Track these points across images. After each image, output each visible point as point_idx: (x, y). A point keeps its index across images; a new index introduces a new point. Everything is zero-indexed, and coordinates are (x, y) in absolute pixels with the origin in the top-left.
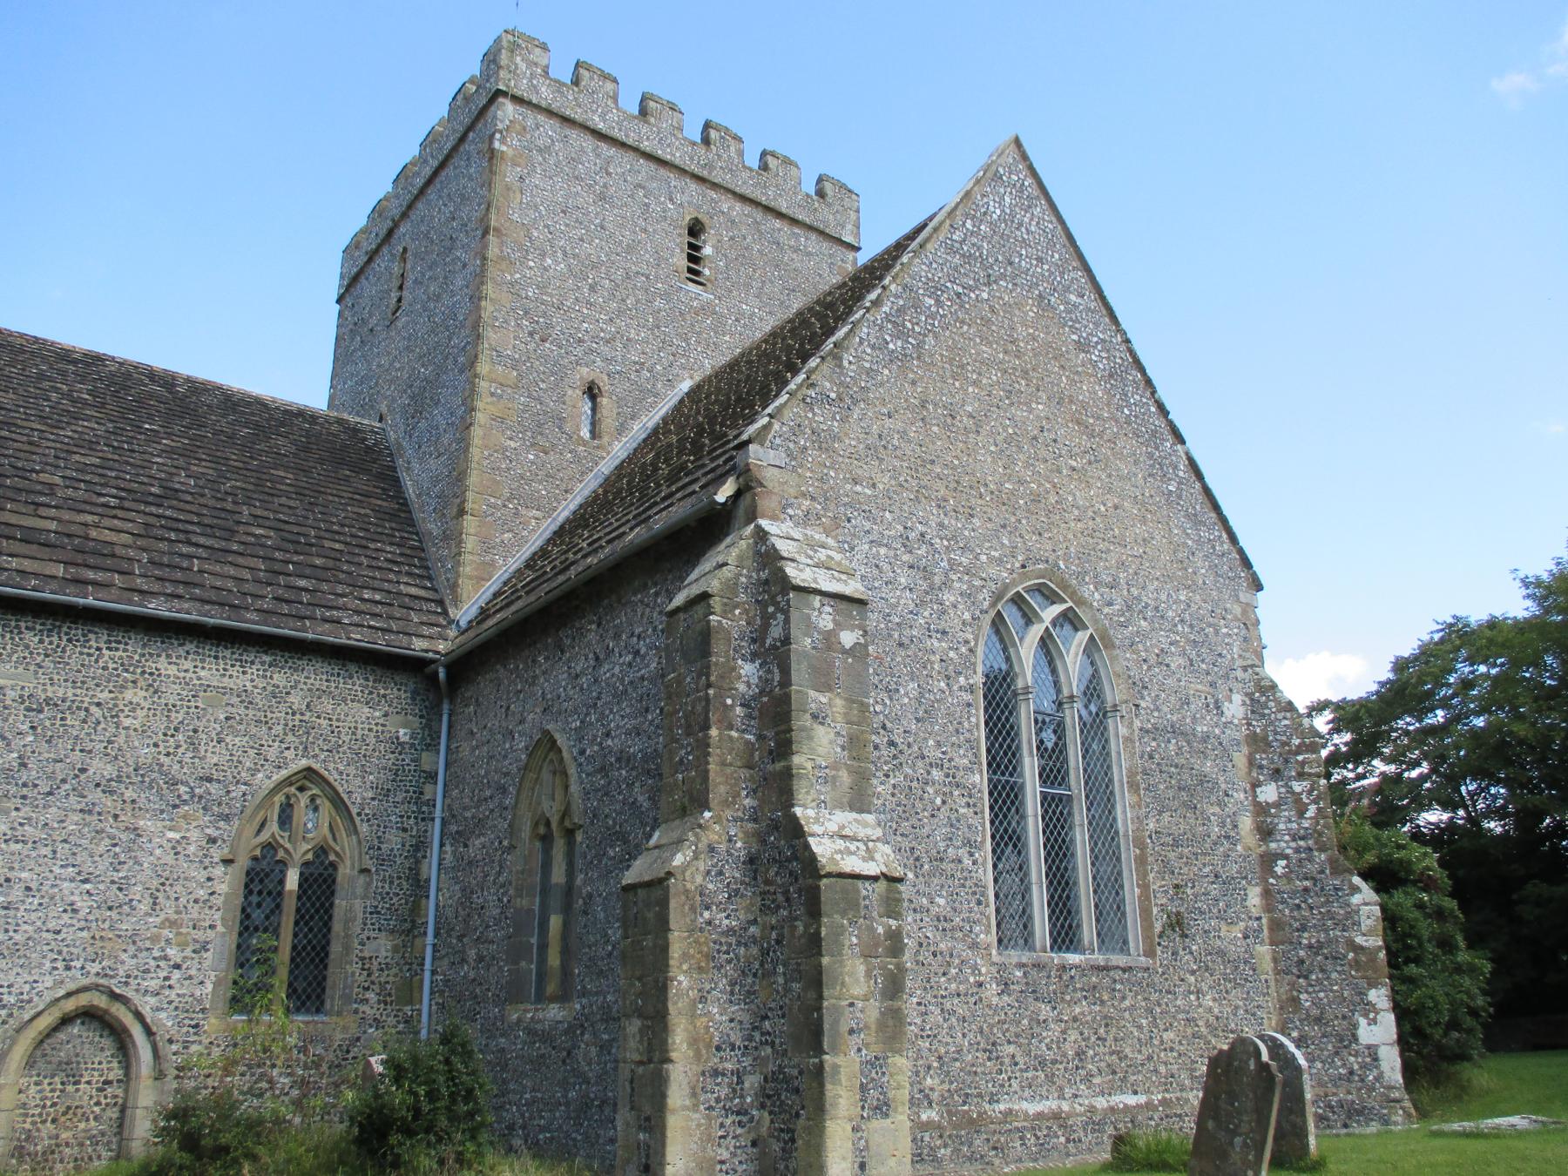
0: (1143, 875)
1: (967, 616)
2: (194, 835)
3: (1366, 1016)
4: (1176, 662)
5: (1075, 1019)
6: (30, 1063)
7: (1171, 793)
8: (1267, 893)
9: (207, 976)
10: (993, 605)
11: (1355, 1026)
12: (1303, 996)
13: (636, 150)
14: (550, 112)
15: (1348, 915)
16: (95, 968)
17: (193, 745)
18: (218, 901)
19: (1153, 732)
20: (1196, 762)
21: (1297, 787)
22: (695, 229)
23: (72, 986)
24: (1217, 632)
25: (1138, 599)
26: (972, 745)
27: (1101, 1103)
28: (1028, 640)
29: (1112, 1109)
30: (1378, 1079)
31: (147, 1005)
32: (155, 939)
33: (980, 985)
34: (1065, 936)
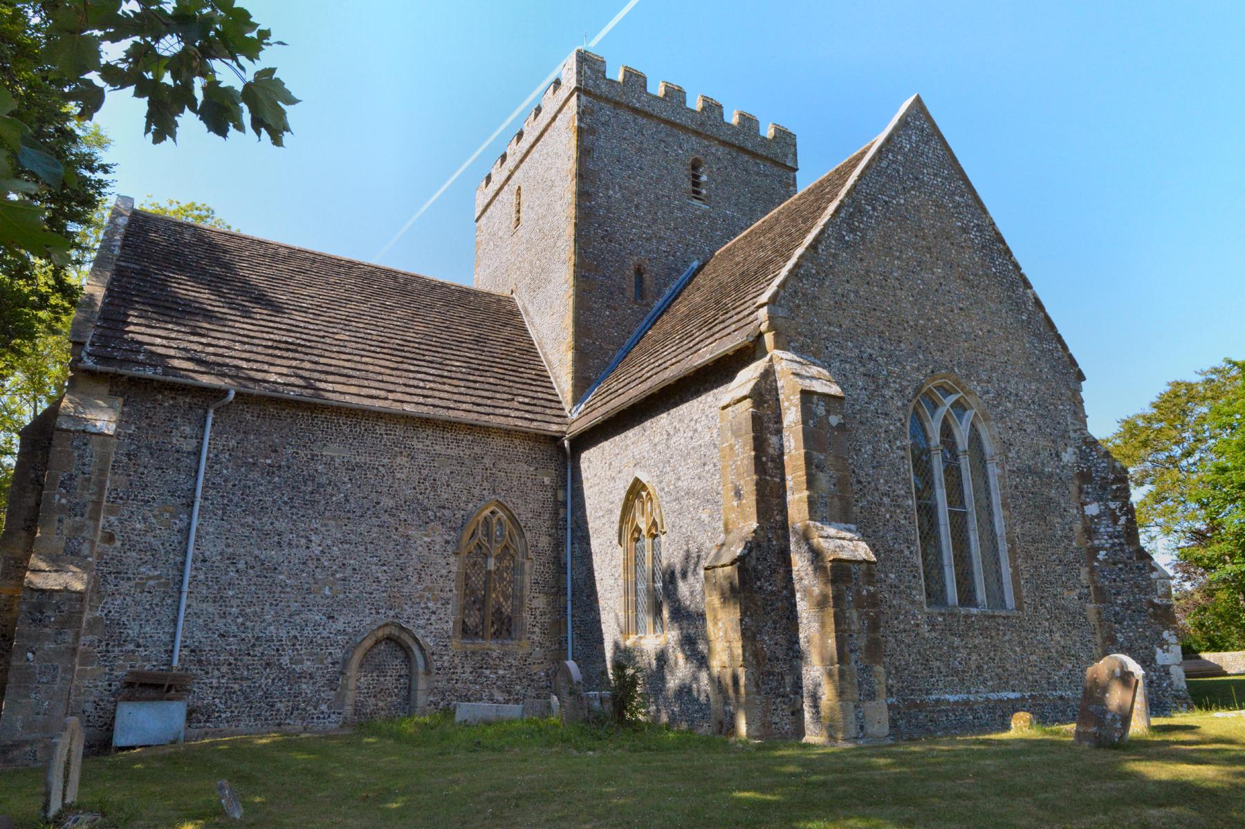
0: (1013, 560)
1: (899, 404)
2: (438, 539)
3: (1161, 647)
4: (1030, 428)
5: (975, 647)
6: (361, 666)
7: (1030, 510)
8: (1092, 570)
9: (448, 620)
10: (915, 397)
11: (1154, 653)
12: (1119, 635)
13: (659, 118)
14: (608, 100)
15: (1149, 585)
16: (392, 613)
17: (434, 488)
18: (453, 576)
19: (1019, 472)
20: (1045, 490)
21: (1112, 505)
22: (695, 166)
23: (381, 623)
24: (1056, 409)
25: (1005, 389)
26: (906, 481)
27: (993, 696)
28: (936, 416)
29: (1001, 700)
30: (1171, 685)
31: (419, 634)
32: (421, 597)
33: (918, 625)
34: (967, 596)
